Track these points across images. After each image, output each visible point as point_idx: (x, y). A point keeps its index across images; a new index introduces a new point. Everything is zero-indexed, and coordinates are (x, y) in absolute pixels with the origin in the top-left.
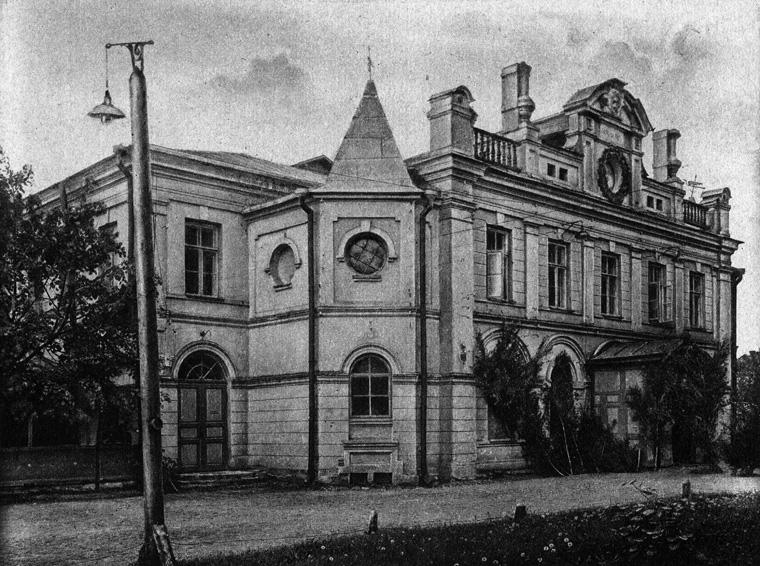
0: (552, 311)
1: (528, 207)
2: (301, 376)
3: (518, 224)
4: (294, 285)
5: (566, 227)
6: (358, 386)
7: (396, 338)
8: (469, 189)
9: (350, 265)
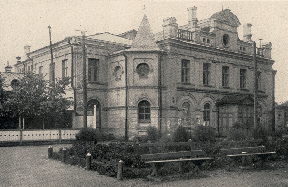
0: (204, 86)
1: (234, 60)
2: (123, 107)
3: (264, 71)
4: (122, 79)
5: (209, 59)
6: (140, 110)
7: (153, 96)
8: (176, 48)
9: (139, 73)
